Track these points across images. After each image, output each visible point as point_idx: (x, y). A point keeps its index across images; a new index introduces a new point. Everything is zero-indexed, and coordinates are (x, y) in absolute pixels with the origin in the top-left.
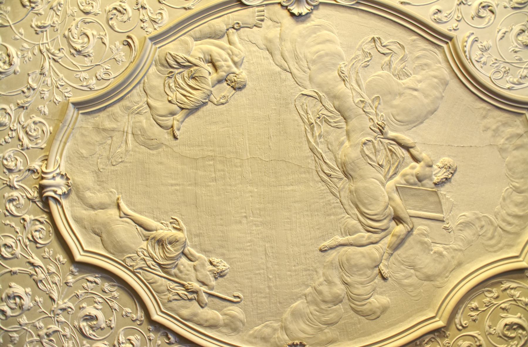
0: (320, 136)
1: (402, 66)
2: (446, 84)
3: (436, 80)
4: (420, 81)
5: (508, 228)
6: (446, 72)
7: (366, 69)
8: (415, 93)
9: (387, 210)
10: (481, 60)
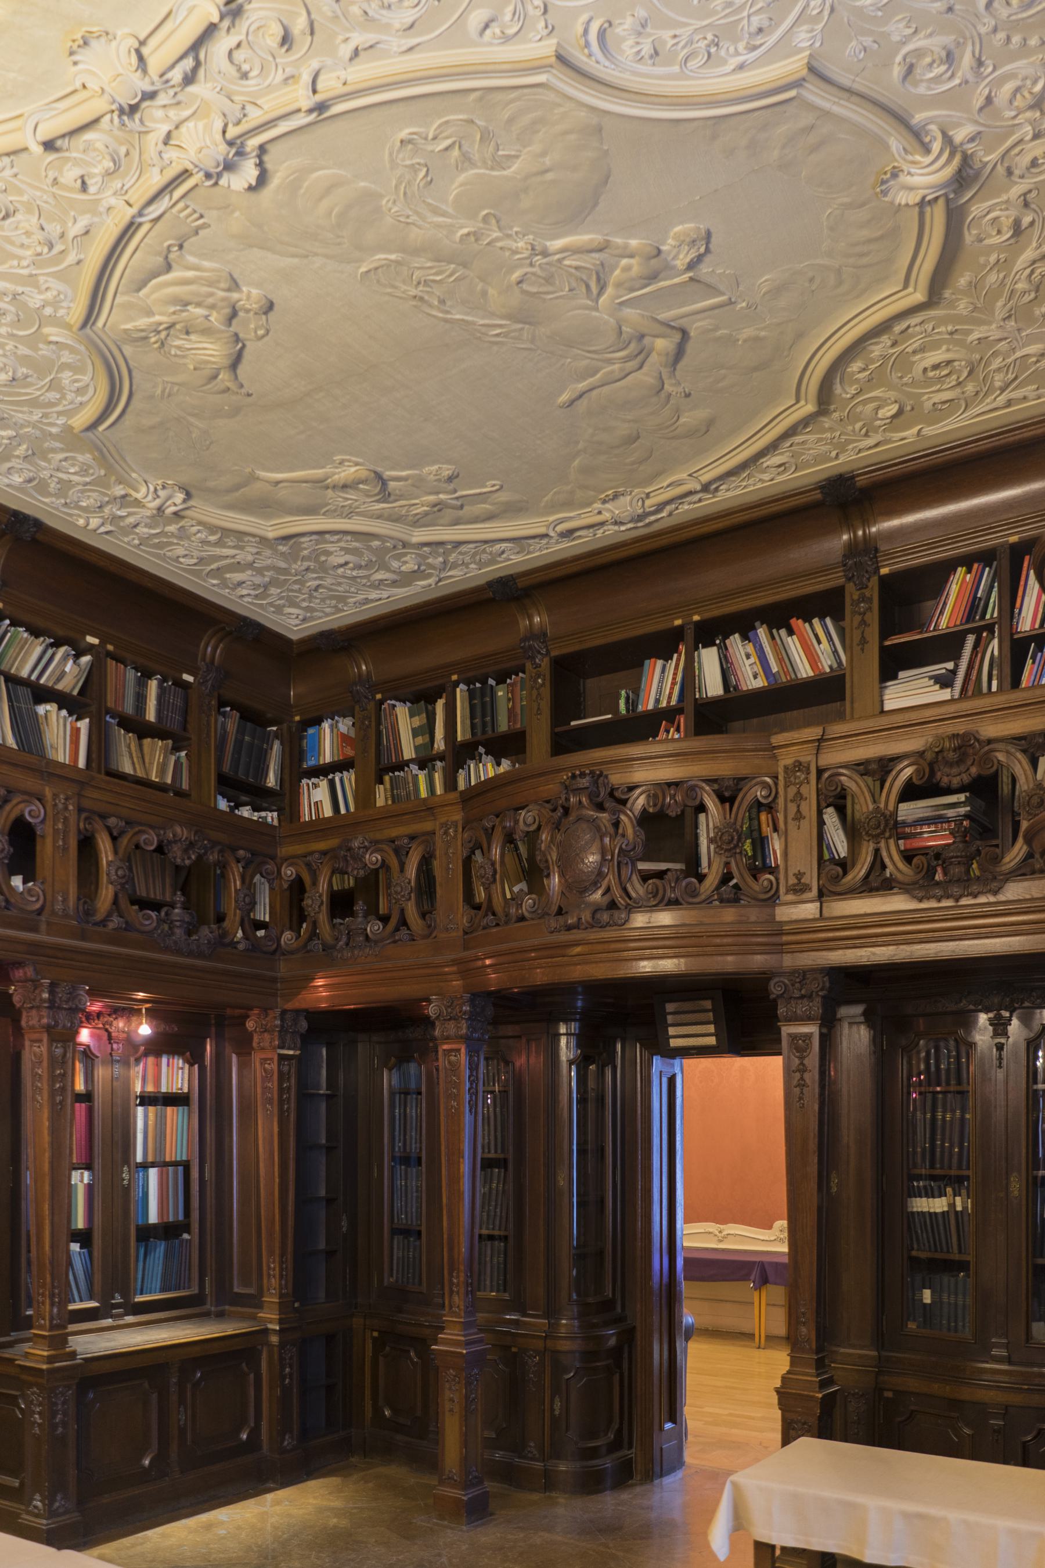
0: (442, 302)
1: (491, 149)
2: (600, 129)
3: (573, 137)
4: (544, 154)
5: (865, 261)
6: (583, 114)
7: (432, 185)
8: (550, 176)
9: (624, 336)
10: (643, 53)
